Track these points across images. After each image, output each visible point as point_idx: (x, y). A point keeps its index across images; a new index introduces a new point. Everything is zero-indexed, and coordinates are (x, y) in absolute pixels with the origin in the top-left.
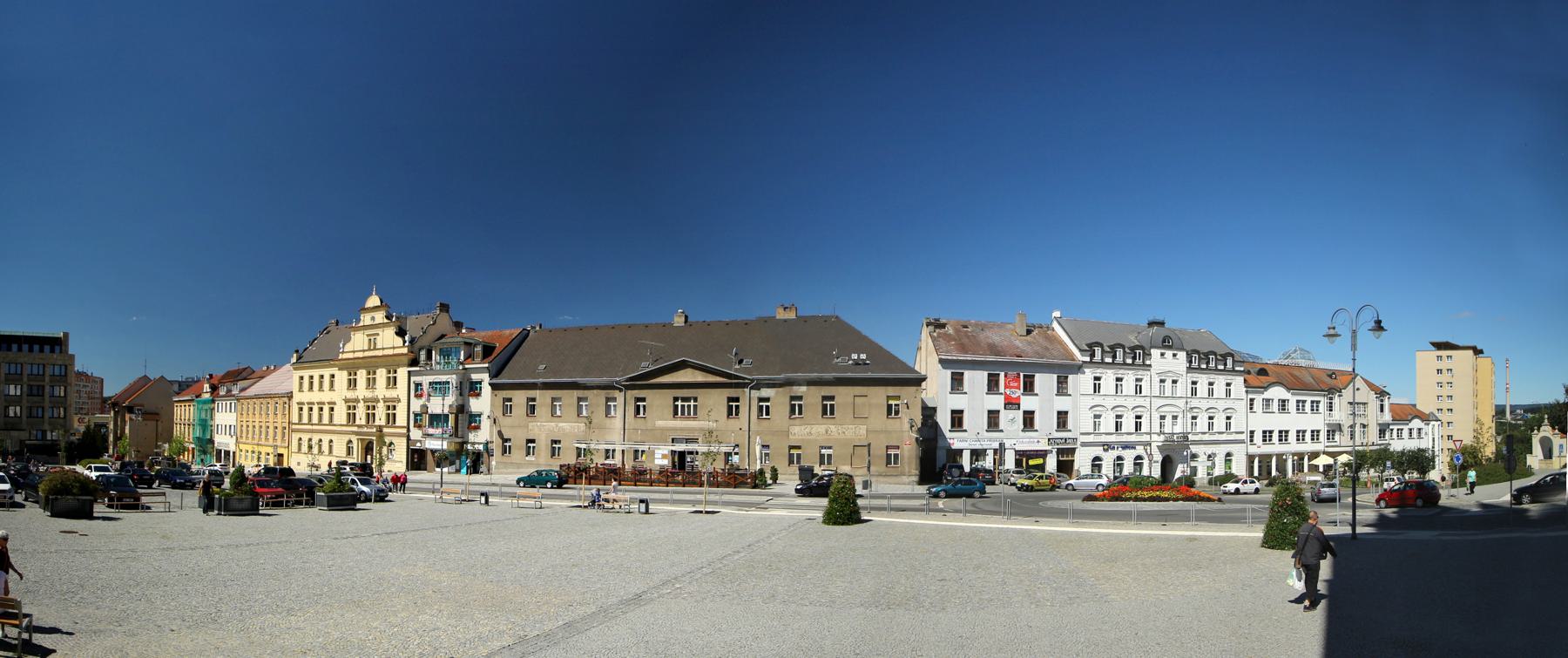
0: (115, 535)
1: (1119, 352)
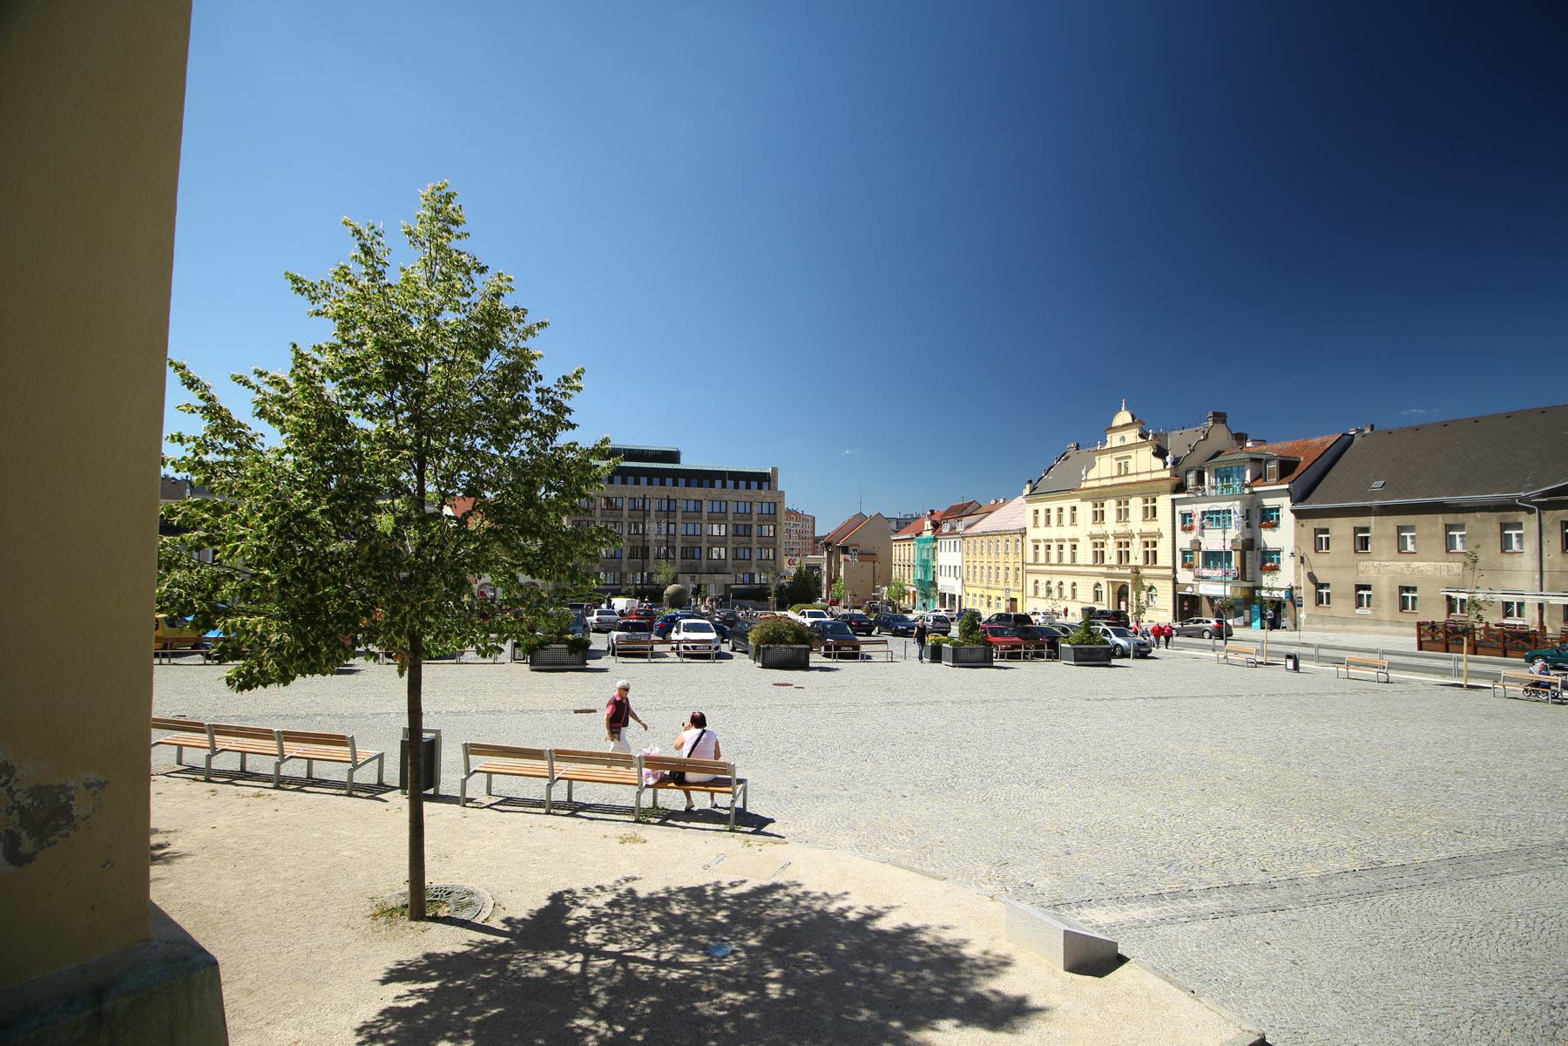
0: (829, 686)
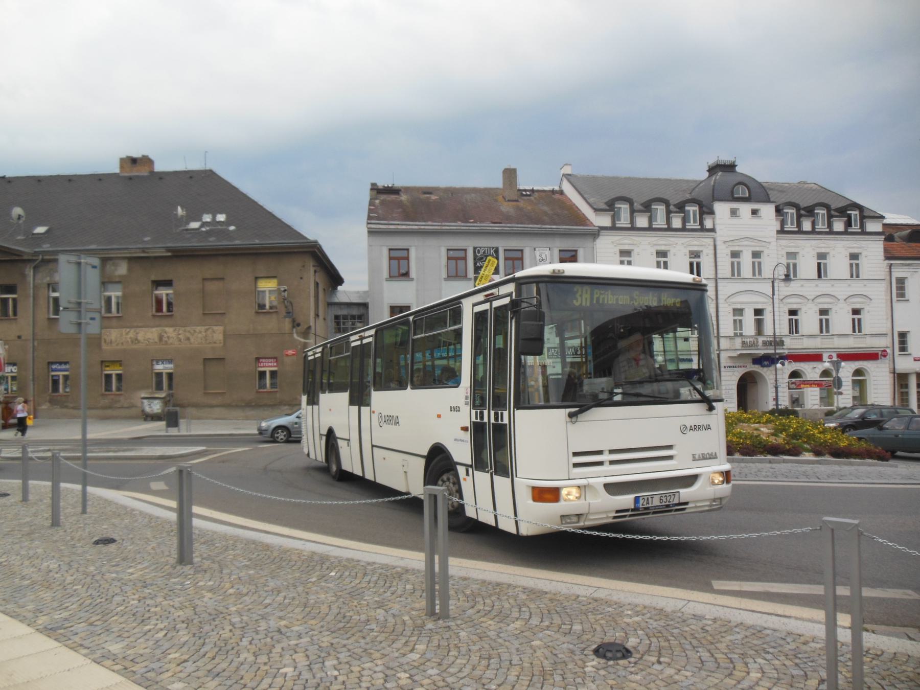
1: (660, 209)
